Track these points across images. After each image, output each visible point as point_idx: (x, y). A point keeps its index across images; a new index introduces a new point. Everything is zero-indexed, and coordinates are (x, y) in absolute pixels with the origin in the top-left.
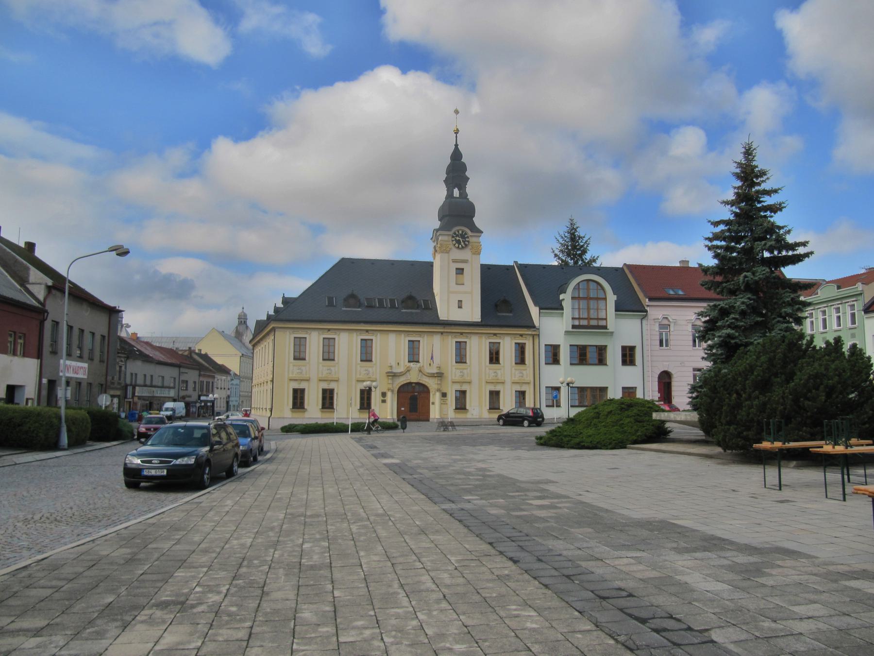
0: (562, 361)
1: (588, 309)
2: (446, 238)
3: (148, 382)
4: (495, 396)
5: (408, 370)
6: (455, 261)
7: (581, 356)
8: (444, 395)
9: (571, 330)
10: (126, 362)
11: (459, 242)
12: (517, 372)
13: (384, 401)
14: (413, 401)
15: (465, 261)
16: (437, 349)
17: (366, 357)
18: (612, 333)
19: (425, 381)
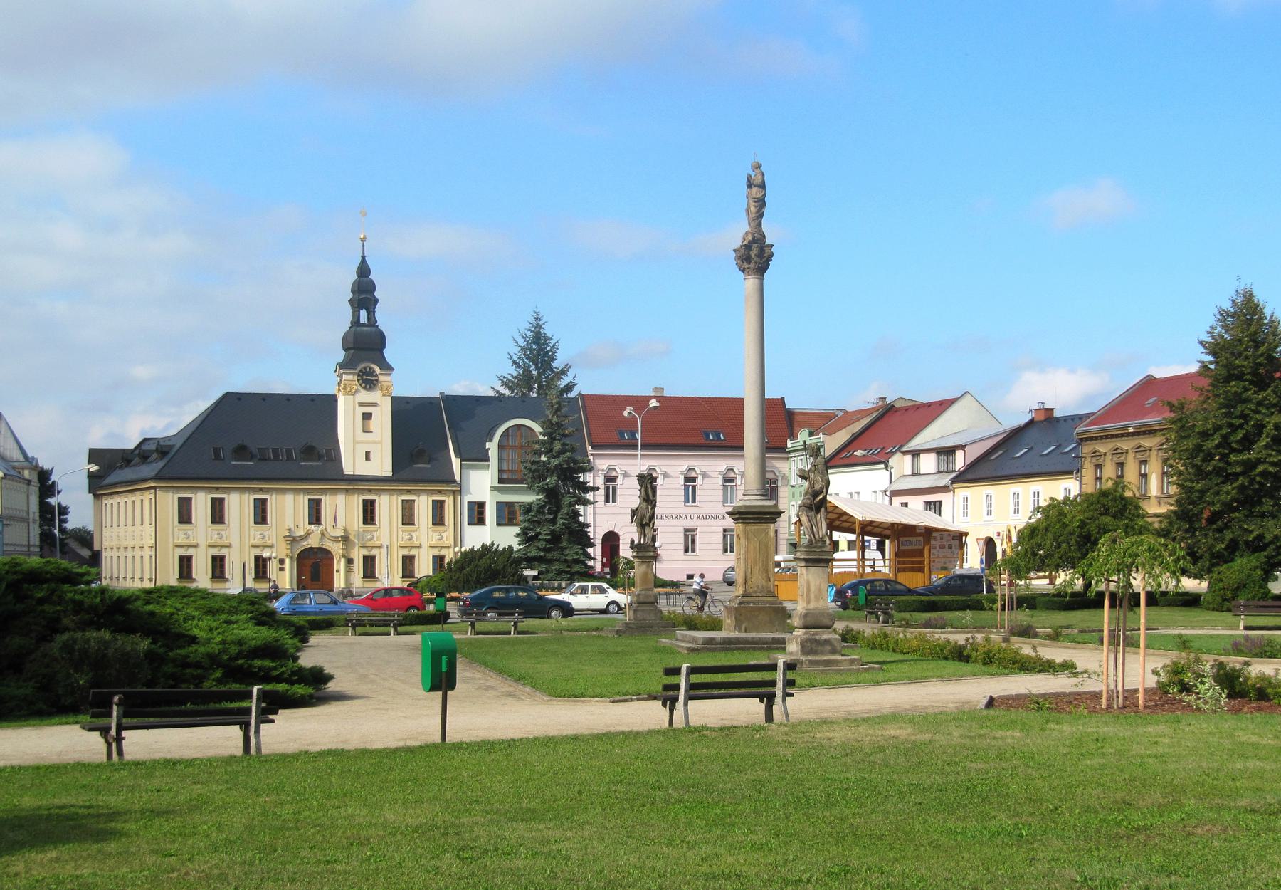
2: (350, 377)
5: (308, 535)
6: (361, 405)
13: (282, 569)
15: (374, 405)
16: (342, 509)
17: (261, 516)
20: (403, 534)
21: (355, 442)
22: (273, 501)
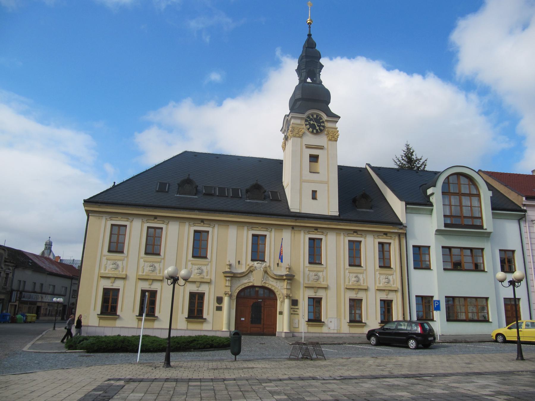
0: (433, 265)
1: (461, 206)
2: (298, 121)
3: (38, 289)
4: (355, 304)
5: (250, 271)
6: (308, 147)
7: (455, 263)
8: (294, 303)
9: (443, 228)
10: (14, 270)
11: (313, 126)
12: (383, 277)
13: (219, 309)
14: (255, 309)
15: (321, 148)
16: (287, 246)
17: (199, 251)
18: (490, 233)
19: (272, 284)
20: (349, 276)
21: (302, 181)
22: (215, 234)
